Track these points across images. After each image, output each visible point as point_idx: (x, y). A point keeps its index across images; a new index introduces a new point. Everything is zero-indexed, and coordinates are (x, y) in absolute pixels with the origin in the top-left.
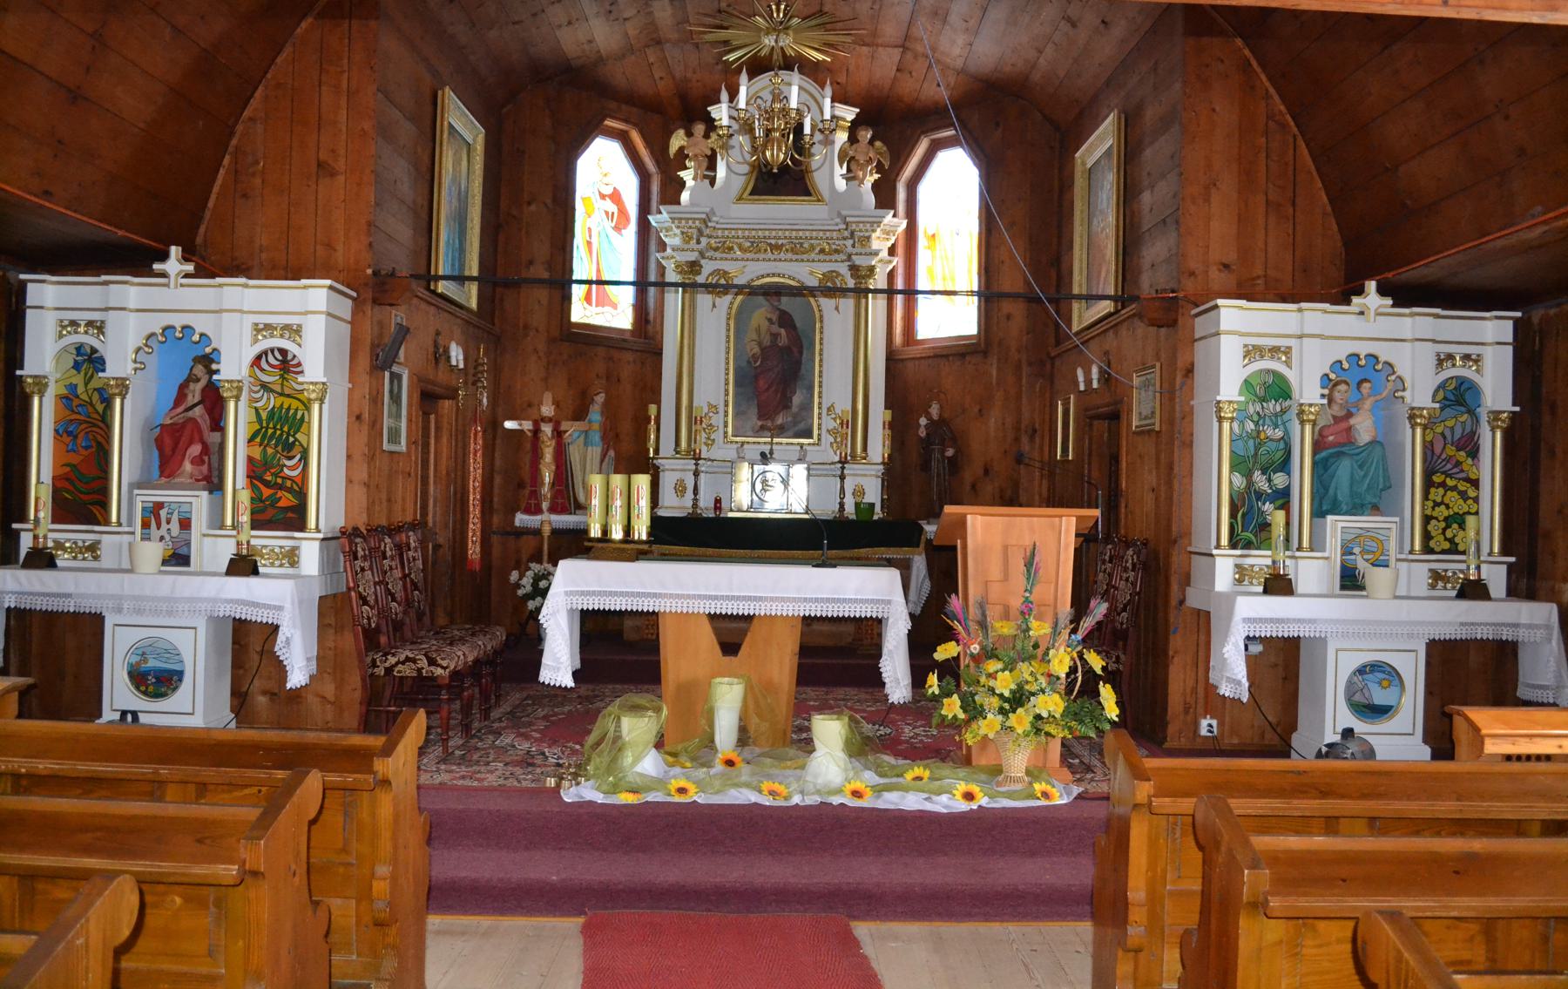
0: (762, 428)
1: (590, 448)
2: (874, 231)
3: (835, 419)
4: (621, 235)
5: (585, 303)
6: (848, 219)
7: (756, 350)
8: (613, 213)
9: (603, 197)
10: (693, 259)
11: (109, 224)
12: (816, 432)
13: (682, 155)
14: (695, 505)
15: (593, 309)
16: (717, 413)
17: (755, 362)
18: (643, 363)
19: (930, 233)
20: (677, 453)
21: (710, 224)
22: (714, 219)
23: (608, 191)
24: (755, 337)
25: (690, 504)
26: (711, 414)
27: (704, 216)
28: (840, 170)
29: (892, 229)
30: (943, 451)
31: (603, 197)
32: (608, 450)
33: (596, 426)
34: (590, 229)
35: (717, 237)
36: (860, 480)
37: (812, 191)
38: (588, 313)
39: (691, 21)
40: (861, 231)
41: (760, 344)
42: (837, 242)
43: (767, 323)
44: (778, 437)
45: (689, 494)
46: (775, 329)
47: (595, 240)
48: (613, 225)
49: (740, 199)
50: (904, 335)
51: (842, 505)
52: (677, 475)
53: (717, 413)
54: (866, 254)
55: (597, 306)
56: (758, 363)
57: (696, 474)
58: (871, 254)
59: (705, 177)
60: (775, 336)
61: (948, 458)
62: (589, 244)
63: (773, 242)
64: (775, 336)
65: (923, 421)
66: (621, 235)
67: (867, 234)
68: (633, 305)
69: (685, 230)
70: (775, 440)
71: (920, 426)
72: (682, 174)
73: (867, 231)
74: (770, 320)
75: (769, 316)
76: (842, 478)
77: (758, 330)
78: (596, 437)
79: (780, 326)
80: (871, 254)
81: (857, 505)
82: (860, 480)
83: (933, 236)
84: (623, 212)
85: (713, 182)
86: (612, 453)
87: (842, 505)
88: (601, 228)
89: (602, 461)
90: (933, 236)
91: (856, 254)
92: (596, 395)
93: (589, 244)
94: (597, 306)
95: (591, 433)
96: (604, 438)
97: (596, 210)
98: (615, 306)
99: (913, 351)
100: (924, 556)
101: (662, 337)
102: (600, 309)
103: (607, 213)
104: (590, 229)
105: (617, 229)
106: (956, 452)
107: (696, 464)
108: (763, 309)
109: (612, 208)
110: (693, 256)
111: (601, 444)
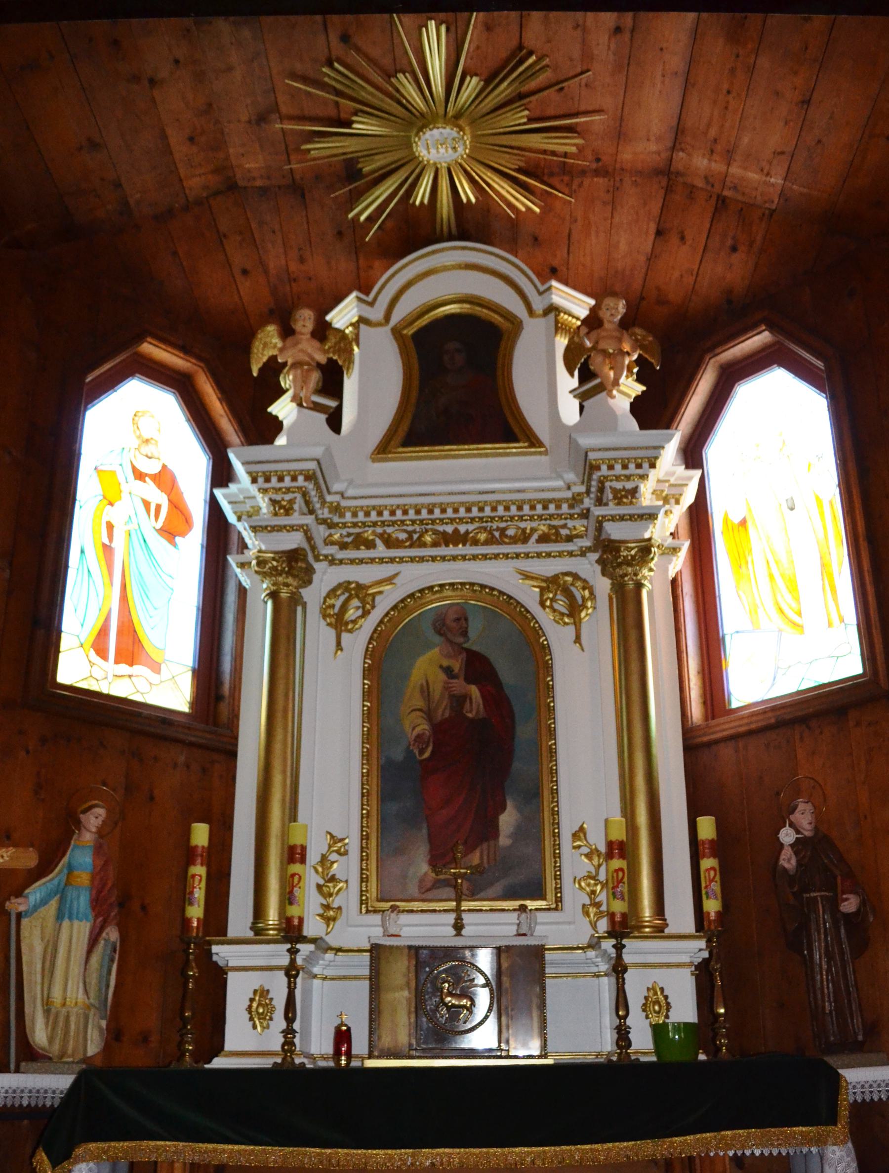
0: (437, 884)
1: (66, 923)
2: (643, 477)
3: (589, 856)
4: (174, 544)
5: (92, 653)
6: (592, 456)
7: (424, 727)
8: (158, 507)
9: (140, 476)
10: (292, 546)
11: (116, 986)
12: (550, 885)
13: (273, 368)
14: (288, 1045)
15: (110, 666)
16: (346, 853)
17: (422, 752)
18: (204, 770)
19: (737, 520)
20: (258, 932)
21: (329, 498)
22: (336, 487)
23: (152, 468)
24: (419, 703)
25: (276, 1042)
26: (333, 857)
27: (312, 465)
28: (567, 382)
29: (674, 491)
30: (833, 904)
31: (140, 476)
32: (102, 929)
33: (84, 878)
34: (110, 527)
35: (345, 525)
36: (660, 977)
37: (517, 430)
38: (97, 673)
39: (284, 110)
40: (618, 478)
41: (429, 714)
42: (570, 523)
43: (442, 676)
44: (473, 897)
45: (279, 1023)
46: (459, 686)
47: (119, 544)
48: (159, 525)
49: (383, 450)
50: (705, 703)
51: (623, 1035)
52: (255, 980)
53: (346, 853)
54: (631, 518)
55: (117, 662)
56: (427, 755)
57: (292, 972)
58: (641, 517)
59: (317, 407)
60: (460, 701)
61: (847, 916)
62: (108, 550)
63: (449, 529)
64: (460, 701)
65: (787, 836)
66: (174, 544)
67: (629, 485)
68: (194, 671)
69: (278, 497)
70: (465, 905)
71: (782, 845)
72: (274, 409)
73: (628, 478)
74: (448, 671)
75: (445, 663)
76: (619, 969)
77: (425, 691)
78: (82, 901)
79: (469, 680)
80: (641, 517)
81: (659, 1031)
82: (660, 977)
83: (743, 523)
84: (178, 507)
85: (335, 421)
86: (112, 934)
87: (623, 1035)
88: (133, 527)
89: (89, 952)
90: (743, 523)
91: (613, 519)
92: (85, 811)
93: (108, 550)
94: (117, 662)
95: (71, 893)
96: (97, 903)
97: (125, 495)
98: (156, 667)
99: (724, 727)
100: (850, 1145)
101: (239, 709)
102: (123, 668)
103: (147, 504)
104: (110, 527)
105: (170, 533)
106: (863, 903)
107: (293, 952)
108: (437, 650)
109: (159, 498)
110: (292, 541)
111: (91, 917)
